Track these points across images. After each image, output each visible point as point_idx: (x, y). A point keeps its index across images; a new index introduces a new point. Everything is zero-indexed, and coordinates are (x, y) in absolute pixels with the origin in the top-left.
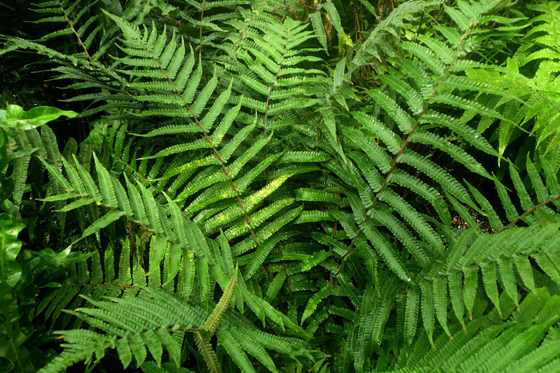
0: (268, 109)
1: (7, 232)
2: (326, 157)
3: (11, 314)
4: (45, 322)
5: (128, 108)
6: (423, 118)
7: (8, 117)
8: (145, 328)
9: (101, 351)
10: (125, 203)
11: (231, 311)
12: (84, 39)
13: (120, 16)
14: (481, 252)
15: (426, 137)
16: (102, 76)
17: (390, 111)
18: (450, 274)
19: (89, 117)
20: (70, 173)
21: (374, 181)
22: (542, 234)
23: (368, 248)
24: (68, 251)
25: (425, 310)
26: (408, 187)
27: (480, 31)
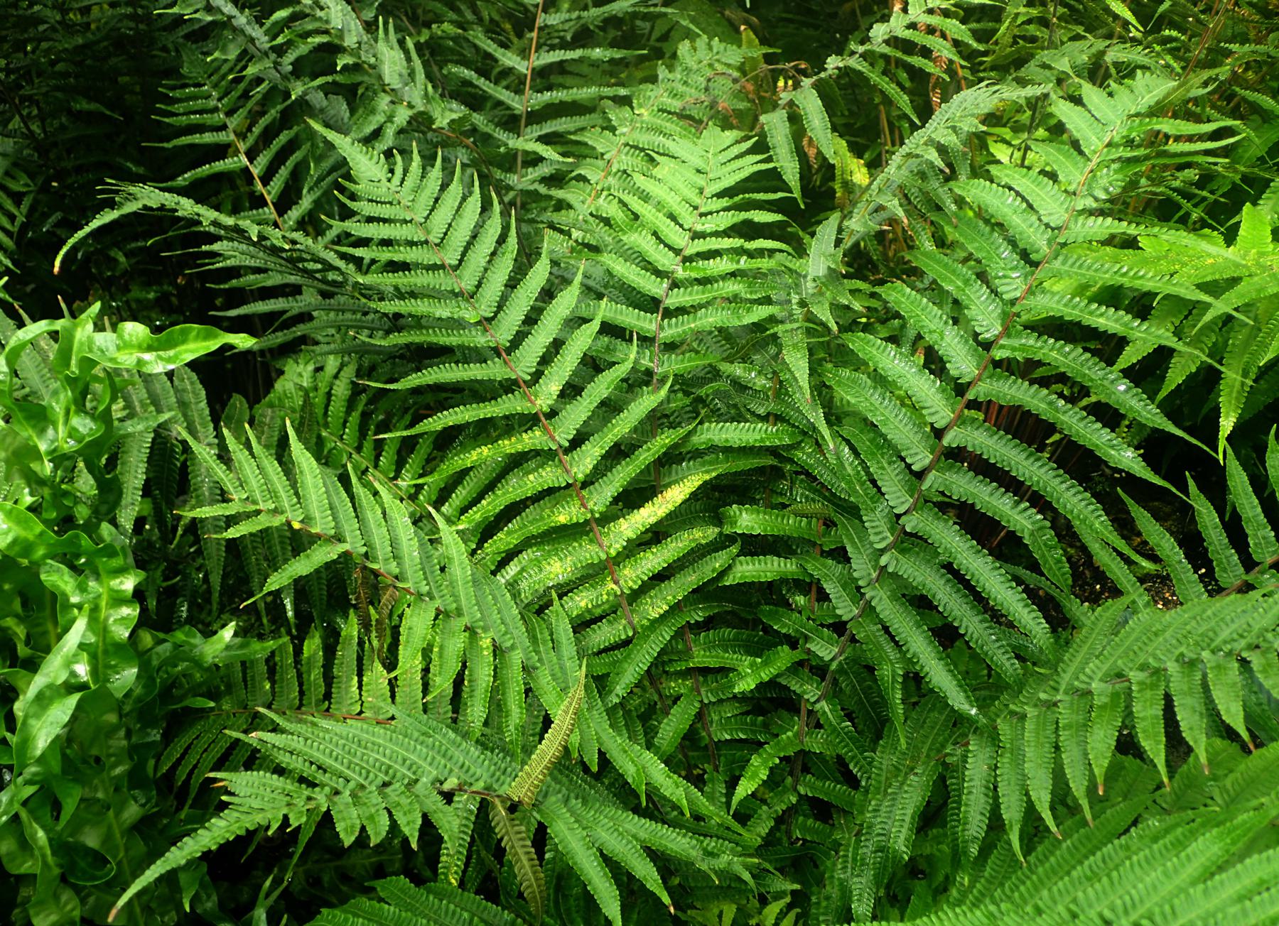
0: (661, 328)
1: (112, 583)
2: (791, 435)
3: (113, 759)
4: (175, 790)
5: (359, 328)
6: (1003, 347)
7: (119, 348)
8: (387, 779)
9: (301, 812)
10: (350, 527)
11: (567, 765)
12: (266, 179)
13: (346, 135)
14: (1135, 648)
15: (1010, 388)
16: (306, 260)
17: (930, 332)
18: (1067, 698)
19: (271, 350)
20: (240, 463)
21: (894, 489)
22: (1271, 608)
23: (883, 639)
24: (227, 633)
25: (1006, 777)
26: (970, 502)
27: (1129, 154)
